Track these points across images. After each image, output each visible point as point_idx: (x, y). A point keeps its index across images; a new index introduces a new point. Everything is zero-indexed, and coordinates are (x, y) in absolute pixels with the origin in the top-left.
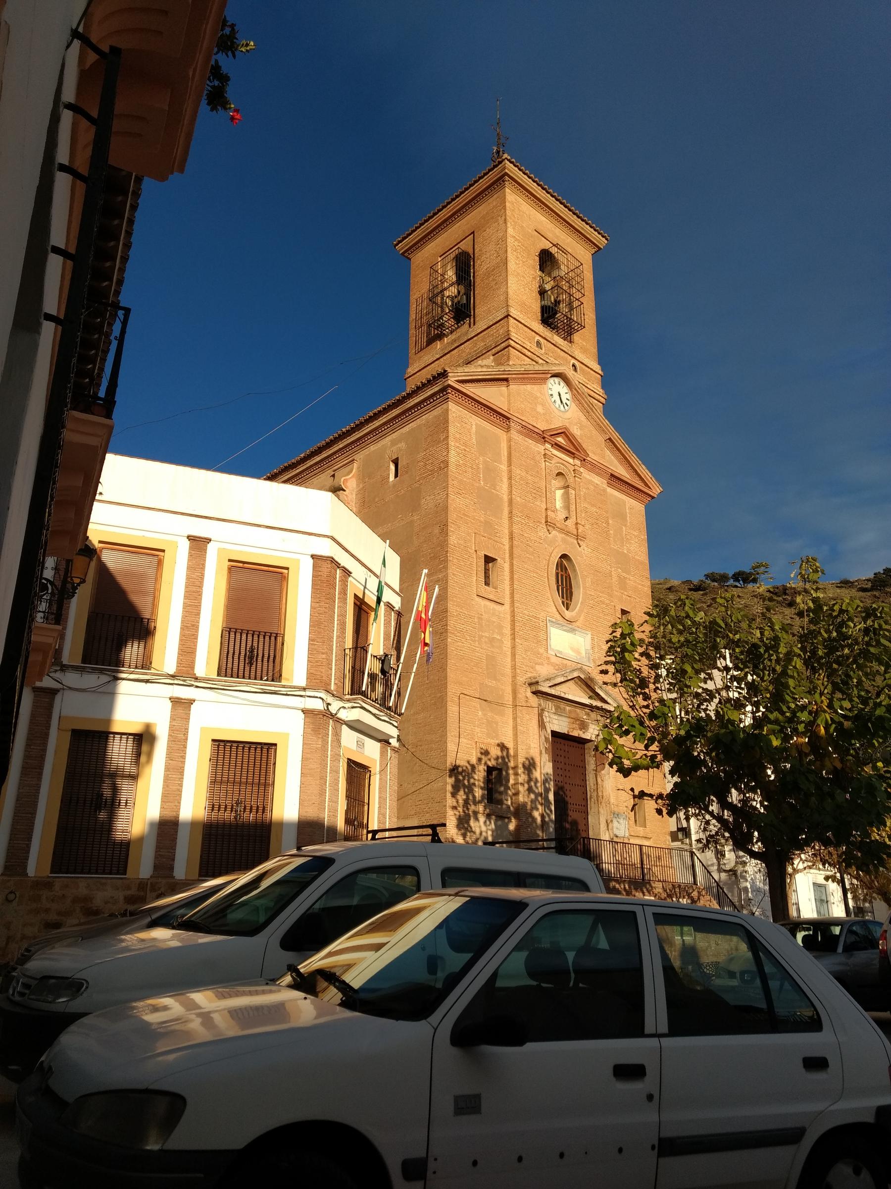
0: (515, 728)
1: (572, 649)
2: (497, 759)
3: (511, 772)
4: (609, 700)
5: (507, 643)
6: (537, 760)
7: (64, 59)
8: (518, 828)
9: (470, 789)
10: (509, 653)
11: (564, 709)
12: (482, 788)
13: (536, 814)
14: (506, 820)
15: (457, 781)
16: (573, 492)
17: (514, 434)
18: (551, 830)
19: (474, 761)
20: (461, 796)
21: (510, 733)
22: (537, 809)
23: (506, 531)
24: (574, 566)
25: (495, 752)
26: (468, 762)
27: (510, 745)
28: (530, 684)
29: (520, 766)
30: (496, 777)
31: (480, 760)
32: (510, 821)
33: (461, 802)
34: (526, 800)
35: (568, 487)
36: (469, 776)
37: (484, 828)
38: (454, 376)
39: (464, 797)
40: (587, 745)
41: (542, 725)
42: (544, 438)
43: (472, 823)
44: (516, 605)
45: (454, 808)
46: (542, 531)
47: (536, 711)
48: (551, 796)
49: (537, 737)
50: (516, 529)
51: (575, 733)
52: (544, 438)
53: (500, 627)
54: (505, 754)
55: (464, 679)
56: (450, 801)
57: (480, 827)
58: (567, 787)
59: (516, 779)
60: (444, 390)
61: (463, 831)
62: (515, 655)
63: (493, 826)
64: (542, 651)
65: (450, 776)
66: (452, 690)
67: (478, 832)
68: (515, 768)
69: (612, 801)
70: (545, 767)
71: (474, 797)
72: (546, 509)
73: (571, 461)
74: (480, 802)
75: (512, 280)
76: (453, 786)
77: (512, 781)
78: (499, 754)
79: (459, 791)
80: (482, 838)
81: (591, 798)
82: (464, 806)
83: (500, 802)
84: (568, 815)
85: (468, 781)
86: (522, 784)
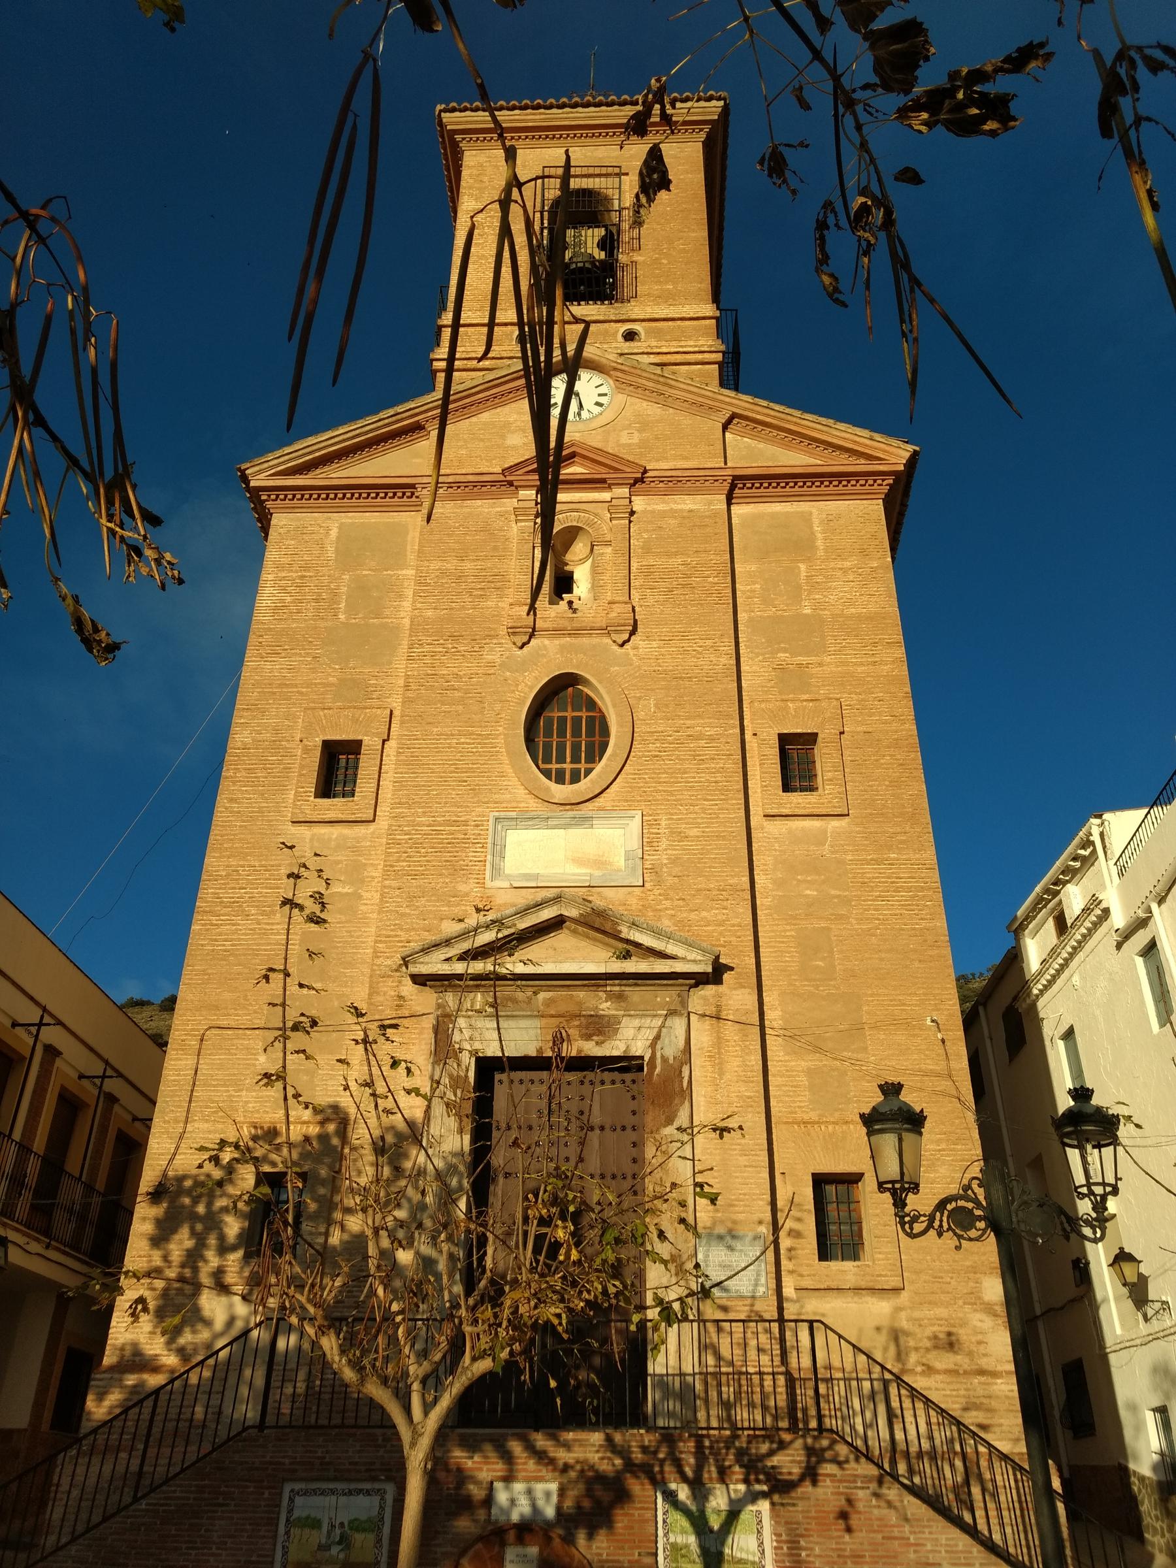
1: (578, 861)
4: (671, 949)
7: (1008, 402)
38: (260, 472)
42: (511, 483)
52: (511, 483)
71: (222, 1238)
73: (606, 496)
74: (234, 1248)
76: (159, 1222)
79: (174, 1231)
85: (209, 1205)
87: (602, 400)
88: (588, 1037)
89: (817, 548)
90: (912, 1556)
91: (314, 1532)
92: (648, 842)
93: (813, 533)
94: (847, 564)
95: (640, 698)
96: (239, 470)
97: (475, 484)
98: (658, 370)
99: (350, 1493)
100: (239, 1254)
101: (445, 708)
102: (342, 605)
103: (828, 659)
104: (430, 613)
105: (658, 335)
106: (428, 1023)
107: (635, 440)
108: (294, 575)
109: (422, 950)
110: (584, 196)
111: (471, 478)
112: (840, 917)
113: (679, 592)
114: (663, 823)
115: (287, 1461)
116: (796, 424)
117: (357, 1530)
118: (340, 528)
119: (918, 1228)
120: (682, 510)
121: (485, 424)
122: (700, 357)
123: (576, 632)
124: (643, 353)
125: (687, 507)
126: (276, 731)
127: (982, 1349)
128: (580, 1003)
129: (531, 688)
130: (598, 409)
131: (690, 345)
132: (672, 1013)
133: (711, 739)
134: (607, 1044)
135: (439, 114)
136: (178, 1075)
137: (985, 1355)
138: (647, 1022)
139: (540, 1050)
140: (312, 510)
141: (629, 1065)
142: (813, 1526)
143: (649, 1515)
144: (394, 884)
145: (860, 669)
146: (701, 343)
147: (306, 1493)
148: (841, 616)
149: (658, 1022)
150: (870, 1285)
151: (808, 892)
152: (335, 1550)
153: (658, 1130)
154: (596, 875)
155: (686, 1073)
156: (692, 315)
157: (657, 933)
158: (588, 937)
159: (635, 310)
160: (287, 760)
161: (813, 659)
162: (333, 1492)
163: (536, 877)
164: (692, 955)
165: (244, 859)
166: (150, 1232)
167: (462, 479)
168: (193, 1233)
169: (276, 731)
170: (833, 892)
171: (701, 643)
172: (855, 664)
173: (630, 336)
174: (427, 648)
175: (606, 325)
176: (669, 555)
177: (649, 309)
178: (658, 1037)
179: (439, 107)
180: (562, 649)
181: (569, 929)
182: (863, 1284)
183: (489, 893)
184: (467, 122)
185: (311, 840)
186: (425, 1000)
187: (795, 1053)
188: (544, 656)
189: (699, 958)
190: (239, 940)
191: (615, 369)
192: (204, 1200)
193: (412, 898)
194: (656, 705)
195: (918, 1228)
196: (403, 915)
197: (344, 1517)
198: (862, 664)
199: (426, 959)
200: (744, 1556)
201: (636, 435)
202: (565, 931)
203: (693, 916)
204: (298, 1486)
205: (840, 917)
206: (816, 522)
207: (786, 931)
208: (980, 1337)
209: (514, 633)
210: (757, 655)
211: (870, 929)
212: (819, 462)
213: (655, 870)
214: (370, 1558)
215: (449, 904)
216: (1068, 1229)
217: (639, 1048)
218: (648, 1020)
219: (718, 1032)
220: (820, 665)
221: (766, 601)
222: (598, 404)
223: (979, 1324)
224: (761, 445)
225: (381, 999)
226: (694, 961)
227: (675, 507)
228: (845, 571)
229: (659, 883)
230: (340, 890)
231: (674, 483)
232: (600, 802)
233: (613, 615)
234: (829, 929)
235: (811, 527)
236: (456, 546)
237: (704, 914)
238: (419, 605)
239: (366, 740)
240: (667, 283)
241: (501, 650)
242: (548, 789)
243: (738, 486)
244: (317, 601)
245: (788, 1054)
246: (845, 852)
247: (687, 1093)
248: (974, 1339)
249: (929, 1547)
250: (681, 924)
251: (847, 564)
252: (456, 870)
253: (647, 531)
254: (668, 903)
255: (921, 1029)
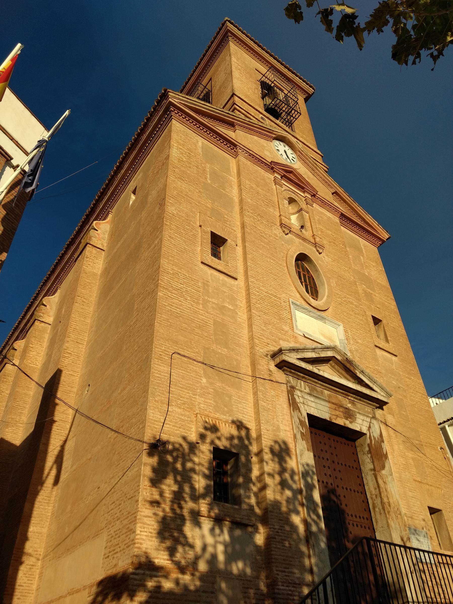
0: (256, 404)
2: (231, 438)
3: (254, 459)
4: (375, 388)
5: (242, 316)
6: (291, 446)
8: (269, 539)
9: (185, 477)
10: (245, 325)
11: (322, 393)
12: (206, 476)
13: (296, 520)
14: (250, 529)
15: (162, 463)
16: (307, 215)
17: (242, 158)
18: (323, 545)
19: (193, 437)
20: (169, 486)
21: (251, 411)
22: (297, 513)
23: (239, 223)
24: (315, 266)
25: (227, 429)
26: (184, 438)
27: (252, 426)
28: (274, 356)
29: (267, 450)
30: (229, 464)
31: (202, 437)
32: (256, 531)
33: (168, 495)
34: (278, 498)
35: (301, 210)
36: (185, 458)
37: (210, 540)
39: (175, 488)
40: (358, 442)
41: (293, 405)
42: (272, 168)
43: (189, 530)
44: (251, 279)
45: (155, 503)
46: (278, 231)
47: (284, 387)
48: (317, 496)
49: (288, 417)
50: (246, 220)
51: (341, 421)
53: (233, 300)
54: (243, 433)
55: (180, 338)
56: (146, 491)
57: (203, 537)
58: (340, 491)
59: (261, 468)
60: (167, 110)
61: (168, 543)
62: (251, 325)
63: (226, 537)
64: (286, 328)
65: (150, 454)
66: (161, 347)
67: (198, 544)
68: (259, 453)
69: (404, 510)
70: (302, 457)
71: (193, 488)
72: (280, 216)
74: (203, 496)
75: (235, 81)
76: (154, 470)
77: (255, 473)
78: (234, 432)
80: (207, 556)
81: (374, 508)
82: (172, 502)
83: (237, 501)
84: (347, 530)
85: (183, 465)
86: (271, 475)
96: (165, 90)
97: (259, 160)
100: (208, 500)
116: (356, 207)
128: (340, 401)
135: (225, 22)
136: (160, 374)
158: (338, 371)
165: (180, 269)
166: (151, 475)
168: (176, 481)
174: (251, 214)
179: (226, 18)
181: (331, 365)
184: (235, 31)
190: (184, 310)
191: (299, 151)
192: (180, 460)
199: (289, 355)
202: (329, 365)
230: (227, 306)
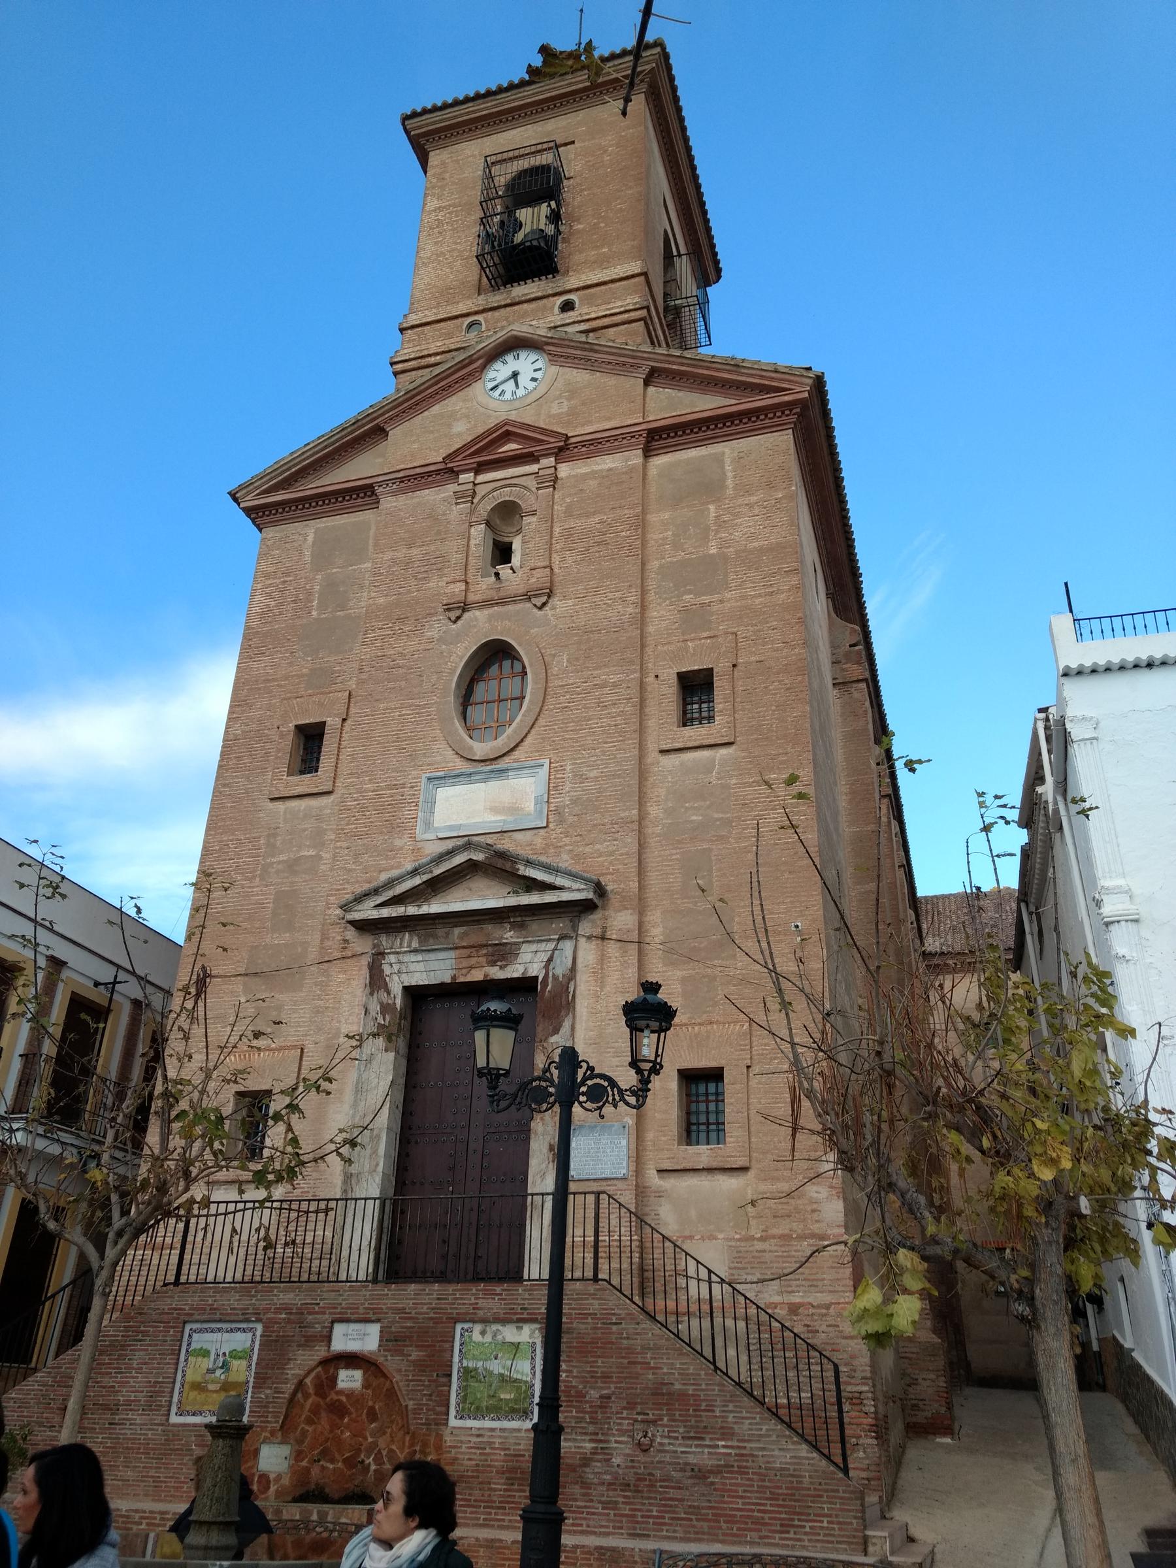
1: (495, 810)
4: (559, 881)
52: (451, 470)
73: (534, 468)
87: (538, 375)
88: (493, 964)
89: (727, 487)
90: (650, 1376)
91: (205, 1359)
92: (553, 787)
93: (724, 474)
94: (754, 499)
95: (554, 655)
98: (583, 338)
99: (232, 1330)
101: (391, 685)
102: (315, 603)
103: (728, 595)
104: (382, 600)
105: (590, 301)
106: (365, 961)
107: (565, 409)
108: (278, 581)
109: (355, 900)
110: (543, 173)
111: (418, 471)
112: (721, 838)
113: (597, 549)
114: (568, 768)
115: (187, 1308)
117: (235, 1358)
118: (315, 533)
119: (503, 1104)
120: (601, 471)
121: (434, 416)
122: (626, 316)
123: (501, 602)
124: (574, 322)
125: (606, 467)
126: (260, 722)
127: (815, 1216)
129: (461, 658)
130: (534, 384)
131: (617, 306)
132: (563, 937)
133: (614, 685)
134: (509, 968)
137: (817, 1221)
138: (543, 946)
139: (454, 977)
140: (292, 520)
141: (526, 986)
142: (574, 1354)
143: (447, 1345)
144: (344, 845)
145: (757, 601)
146: (628, 301)
147: (200, 1331)
148: (744, 551)
149: (552, 945)
150: (721, 1165)
151: (694, 818)
152: (218, 1373)
153: (546, 1039)
154: (509, 822)
155: (571, 989)
156: (622, 275)
157: (547, 868)
159: (573, 281)
160: (268, 746)
161: (717, 597)
162: (219, 1330)
163: (459, 827)
164: (576, 886)
165: (233, 834)
167: (412, 472)
169: (260, 722)
170: (716, 816)
171: (611, 595)
172: (754, 596)
173: (567, 307)
175: (545, 301)
176: (588, 515)
177: (584, 277)
178: (550, 960)
180: (490, 618)
182: (715, 1165)
183: (420, 845)
185: (285, 812)
186: (363, 945)
187: (672, 964)
188: (475, 626)
189: (583, 887)
193: (357, 855)
194: (568, 660)
195: (503, 1104)
196: (350, 870)
197: (226, 1349)
198: (760, 596)
199: (360, 907)
200: (519, 1377)
201: (566, 403)
203: (588, 849)
204: (195, 1326)
205: (721, 838)
206: (728, 460)
207: (672, 855)
208: (815, 1206)
209: (449, 610)
210: (666, 599)
211: (746, 847)
212: (734, 402)
213: (558, 812)
214: (242, 1379)
215: (387, 858)
216: (617, 1098)
217: (535, 970)
218: (544, 944)
219: (603, 950)
220: (722, 601)
221: (677, 546)
222: (534, 380)
223: (816, 1195)
224: (681, 394)
225: (330, 943)
226: (578, 890)
227: (595, 468)
228: (750, 506)
229: (561, 822)
230: (306, 853)
231: (595, 445)
232: (516, 754)
233: (534, 580)
234: (710, 850)
235: (723, 467)
236: (407, 535)
237: (598, 846)
238: (373, 595)
239: (329, 720)
240: (602, 246)
241: (438, 627)
242: (471, 748)
243: (656, 439)
244: (295, 602)
245: (665, 965)
246: (730, 777)
247: (570, 1006)
248: (809, 1209)
249: (665, 1370)
250: (577, 857)
251: (754, 499)
252: (394, 828)
253: (570, 495)
254: (567, 840)
255: (785, 935)
